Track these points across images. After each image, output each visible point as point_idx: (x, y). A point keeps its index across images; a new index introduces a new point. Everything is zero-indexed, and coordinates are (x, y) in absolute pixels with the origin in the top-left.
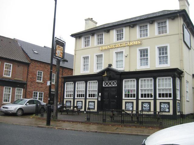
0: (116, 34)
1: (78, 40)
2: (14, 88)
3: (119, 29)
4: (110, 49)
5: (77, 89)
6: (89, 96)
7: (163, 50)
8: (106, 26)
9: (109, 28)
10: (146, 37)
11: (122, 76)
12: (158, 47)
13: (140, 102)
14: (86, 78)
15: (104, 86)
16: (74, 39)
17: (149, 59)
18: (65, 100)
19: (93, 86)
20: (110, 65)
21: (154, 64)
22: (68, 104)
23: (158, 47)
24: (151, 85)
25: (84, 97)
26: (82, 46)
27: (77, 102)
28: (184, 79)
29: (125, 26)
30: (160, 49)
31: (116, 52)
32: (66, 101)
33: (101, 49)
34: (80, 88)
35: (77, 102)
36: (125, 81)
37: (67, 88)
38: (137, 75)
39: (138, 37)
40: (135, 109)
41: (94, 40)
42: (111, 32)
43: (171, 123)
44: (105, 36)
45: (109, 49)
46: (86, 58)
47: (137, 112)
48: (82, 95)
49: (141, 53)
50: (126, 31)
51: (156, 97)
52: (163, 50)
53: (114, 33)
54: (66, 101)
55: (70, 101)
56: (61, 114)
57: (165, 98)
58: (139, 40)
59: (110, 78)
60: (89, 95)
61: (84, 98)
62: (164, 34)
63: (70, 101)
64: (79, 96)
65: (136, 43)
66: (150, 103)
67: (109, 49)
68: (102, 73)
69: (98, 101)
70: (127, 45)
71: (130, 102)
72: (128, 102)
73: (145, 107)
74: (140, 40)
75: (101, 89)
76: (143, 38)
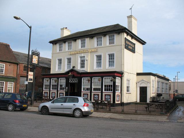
0: (81, 42)
1: (54, 45)
2: (7, 82)
3: (83, 39)
4: (76, 54)
5: (60, 83)
6: (94, 90)
7: (111, 56)
8: (90, 34)
9: (76, 38)
10: (100, 46)
11: (82, 75)
12: (108, 54)
13: (92, 94)
14: (58, 76)
15: (70, 82)
16: (51, 44)
17: (102, 63)
18: (44, 92)
19: (63, 82)
20: (74, 67)
21: (106, 67)
22: (46, 95)
23: (108, 54)
24: (100, 83)
25: (89, 90)
26: (57, 50)
27: (52, 93)
28: (124, 78)
29: (87, 38)
30: (110, 55)
31: (81, 56)
32: (45, 92)
33: (70, 53)
34: (62, 83)
35: (52, 93)
36: (105, 78)
37: (60, 82)
38: (91, 75)
39: (96, 46)
40: (100, 99)
41: (66, 46)
42: (77, 41)
43: (132, 111)
44: (73, 44)
45: (75, 54)
46: (60, 61)
47: (102, 102)
48: (87, 89)
49: (109, 57)
50: (87, 40)
51: (81, 90)
52: (112, 57)
53: (79, 42)
54: (45, 92)
55: (47, 93)
56: (36, 102)
57: (108, 92)
58: (95, 48)
59: (73, 77)
60: (94, 89)
61: (57, 90)
62: (113, 45)
63: (47, 93)
64: (95, 89)
65: (94, 50)
66: (98, 95)
67: (75, 54)
68: (68, 73)
69: (66, 92)
70: (87, 51)
71: (86, 94)
72: (85, 94)
73: (96, 98)
74: (97, 48)
75: (67, 84)
76: (99, 46)
